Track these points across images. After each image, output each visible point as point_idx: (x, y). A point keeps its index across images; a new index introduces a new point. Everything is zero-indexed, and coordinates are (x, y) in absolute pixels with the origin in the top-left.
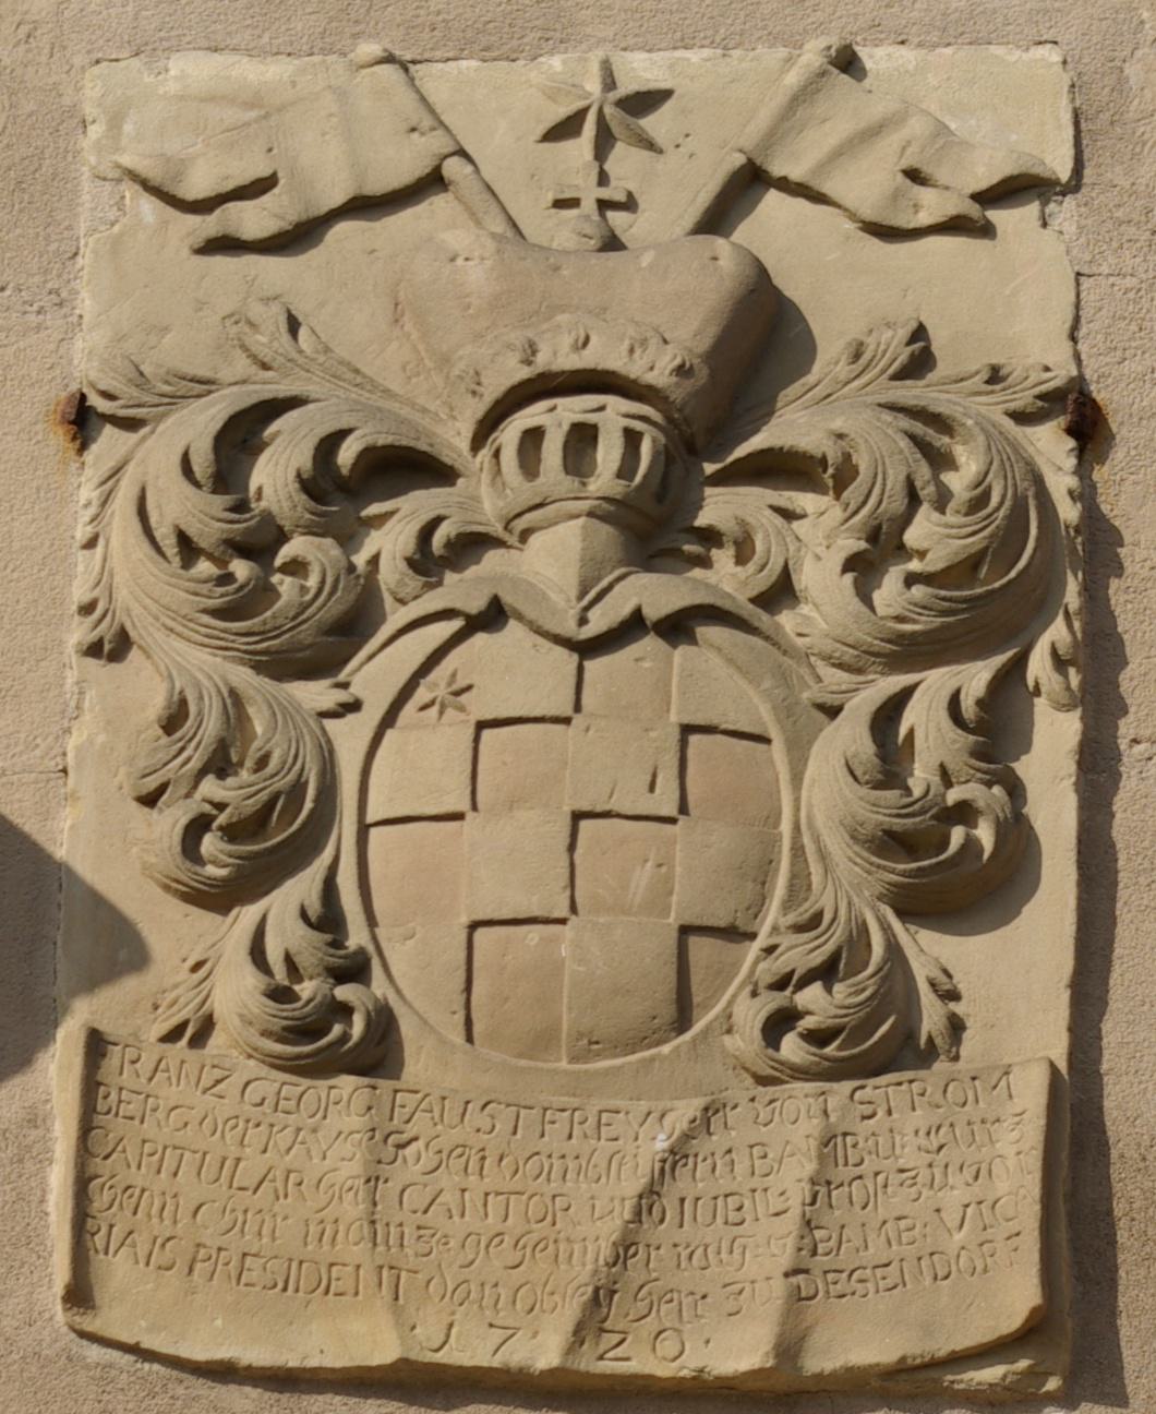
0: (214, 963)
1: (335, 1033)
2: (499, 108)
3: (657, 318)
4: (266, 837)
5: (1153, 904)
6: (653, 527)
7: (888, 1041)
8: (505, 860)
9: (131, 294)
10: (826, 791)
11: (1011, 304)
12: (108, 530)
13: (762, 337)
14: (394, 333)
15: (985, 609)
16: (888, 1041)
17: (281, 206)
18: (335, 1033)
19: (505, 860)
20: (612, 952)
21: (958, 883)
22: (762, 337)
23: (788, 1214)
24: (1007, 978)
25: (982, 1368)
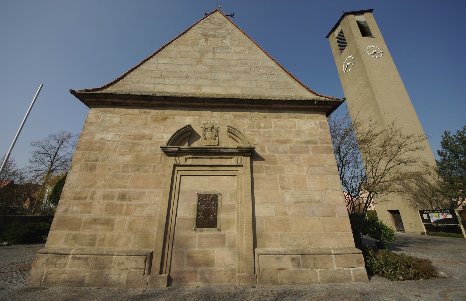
0: (203, 138)
1: (205, 139)
2: (209, 122)
3: (211, 126)
4: (204, 135)
5: (222, 253)
6: (211, 130)
7: (215, 139)
8: (208, 136)
9: (202, 125)
10: (214, 135)
11: (218, 126)
12: (202, 130)
13: (213, 126)
14: (207, 126)
15: (217, 131)
16: (215, 139)
17: (245, 174)
18: (205, 139)
19: (208, 136)
20: (210, 138)
21: (216, 136)
22: (213, 126)
23: (237, 143)
24: (217, 138)
25: (260, 112)
